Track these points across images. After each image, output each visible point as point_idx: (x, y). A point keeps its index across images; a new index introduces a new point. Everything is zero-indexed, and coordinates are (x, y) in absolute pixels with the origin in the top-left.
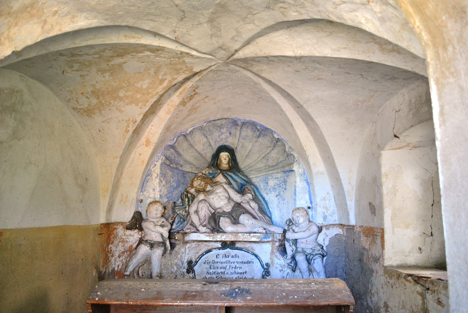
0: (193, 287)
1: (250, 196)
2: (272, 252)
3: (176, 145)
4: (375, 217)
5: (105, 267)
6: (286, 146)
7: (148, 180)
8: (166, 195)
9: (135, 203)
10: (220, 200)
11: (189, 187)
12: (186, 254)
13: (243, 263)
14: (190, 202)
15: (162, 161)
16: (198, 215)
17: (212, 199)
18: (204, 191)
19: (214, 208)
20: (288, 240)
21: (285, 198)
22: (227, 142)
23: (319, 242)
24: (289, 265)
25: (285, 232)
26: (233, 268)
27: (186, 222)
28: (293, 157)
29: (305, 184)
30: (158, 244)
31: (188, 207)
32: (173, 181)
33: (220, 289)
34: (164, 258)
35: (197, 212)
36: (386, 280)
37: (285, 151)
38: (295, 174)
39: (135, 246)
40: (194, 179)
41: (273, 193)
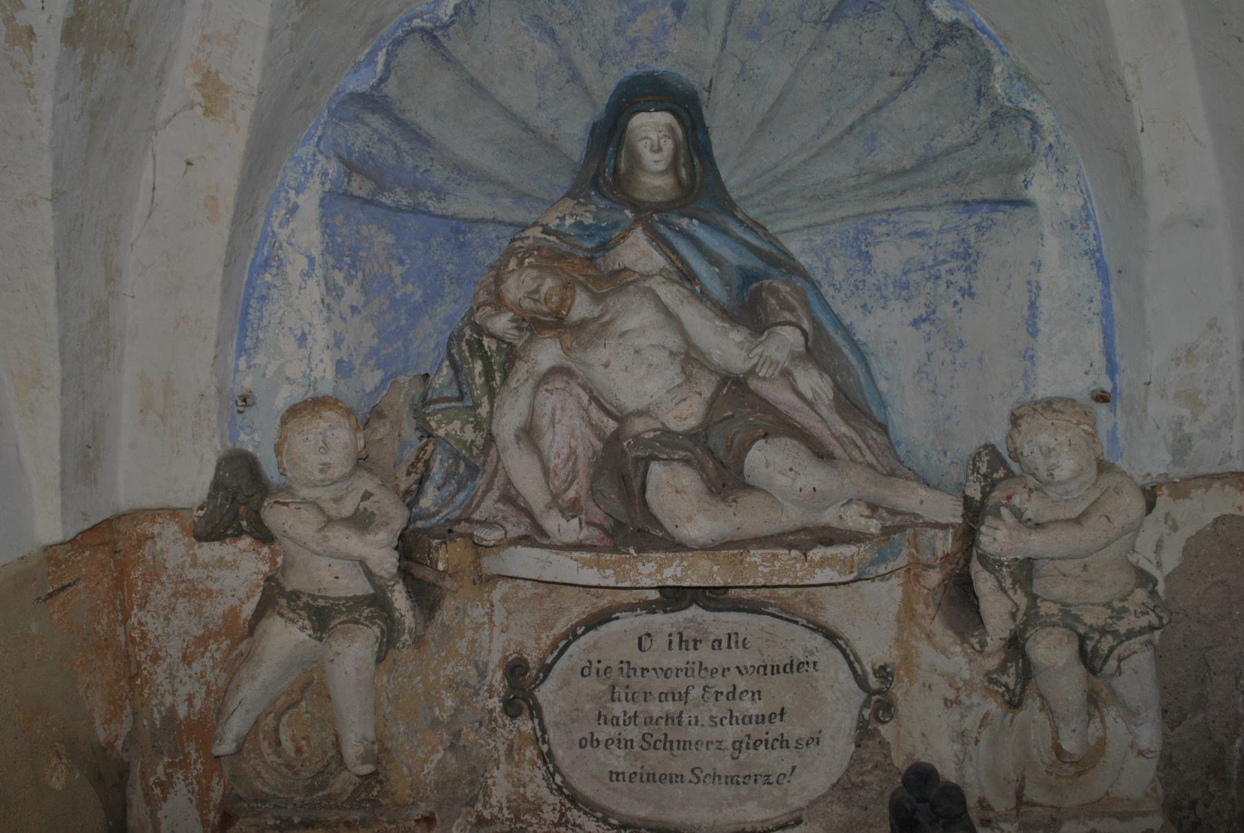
1: (788, 339)
2: (907, 615)
3: (391, 88)
5: (128, 710)
6: (997, 69)
7: (264, 291)
8: (373, 352)
11: (484, 304)
12: (496, 631)
14: (498, 375)
15: (328, 186)
16: (537, 449)
17: (600, 369)
19: (613, 410)
22: (664, 54)
24: (991, 681)
25: (974, 513)
26: (722, 698)
27: (481, 481)
28: (1028, 129)
29: (1085, 274)
30: (350, 610)
31: (485, 399)
32: (405, 279)
35: (529, 434)
37: (980, 94)
39: (248, 609)
40: (506, 266)
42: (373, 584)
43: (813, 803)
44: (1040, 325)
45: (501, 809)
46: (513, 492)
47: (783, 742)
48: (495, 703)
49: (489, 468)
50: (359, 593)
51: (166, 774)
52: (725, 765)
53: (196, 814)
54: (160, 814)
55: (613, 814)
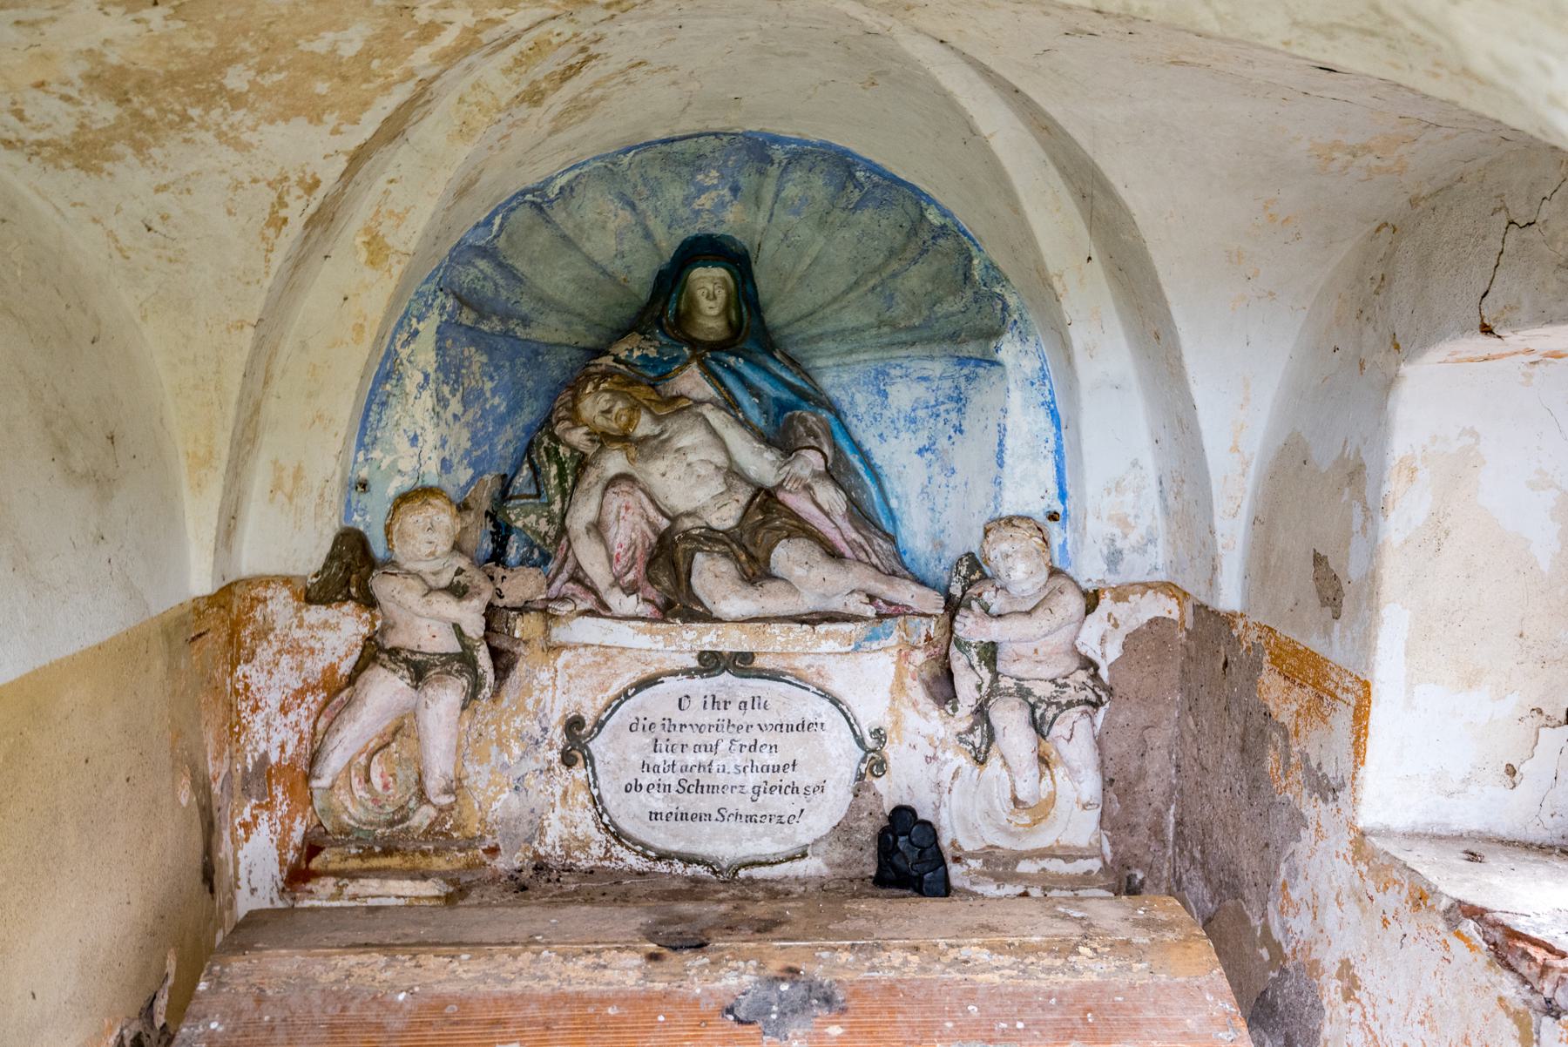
0: (608, 972)
2: (899, 686)
3: (501, 243)
4: (1337, 625)
6: (976, 262)
7: (384, 399)
8: (468, 453)
9: (336, 499)
10: (693, 481)
11: (563, 419)
12: (558, 693)
13: (785, 727)
14: (570, 479)
15: (445, 317)
16: (603, 540)
18: (624, 439)
19: (666, 510)
20: (962, 646)
21: (957, 467)
22: (723, 222)
23: (1082, 650)
24: (961, 741)
27: (552, 566)
29: (1043, 421)
30: (443, 664)
31: (558, 498)
32: (494, 392)
33: (717, 984)
34: (472, 718)
35: (597, 528)
36: (1357, 882)
38: (1003, 377)
39: (345, 668)
41: (907, 440)
42: (464, 646)
43: (816, 842)
44: (1006, 458)
45: (554, 847)
46: (581, 574)
47: (795, 789)
48: (555, 755)
49: (560, 555)
50: (451, 651)
51: (252, 815)
52: (746, 808)
53: (276, 853)
54: (240, 854)
55: (651, 848)
